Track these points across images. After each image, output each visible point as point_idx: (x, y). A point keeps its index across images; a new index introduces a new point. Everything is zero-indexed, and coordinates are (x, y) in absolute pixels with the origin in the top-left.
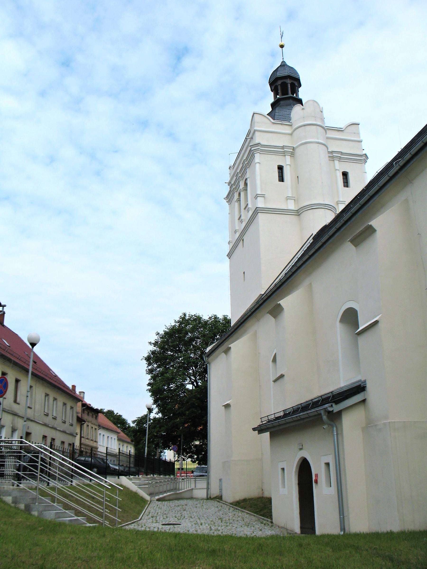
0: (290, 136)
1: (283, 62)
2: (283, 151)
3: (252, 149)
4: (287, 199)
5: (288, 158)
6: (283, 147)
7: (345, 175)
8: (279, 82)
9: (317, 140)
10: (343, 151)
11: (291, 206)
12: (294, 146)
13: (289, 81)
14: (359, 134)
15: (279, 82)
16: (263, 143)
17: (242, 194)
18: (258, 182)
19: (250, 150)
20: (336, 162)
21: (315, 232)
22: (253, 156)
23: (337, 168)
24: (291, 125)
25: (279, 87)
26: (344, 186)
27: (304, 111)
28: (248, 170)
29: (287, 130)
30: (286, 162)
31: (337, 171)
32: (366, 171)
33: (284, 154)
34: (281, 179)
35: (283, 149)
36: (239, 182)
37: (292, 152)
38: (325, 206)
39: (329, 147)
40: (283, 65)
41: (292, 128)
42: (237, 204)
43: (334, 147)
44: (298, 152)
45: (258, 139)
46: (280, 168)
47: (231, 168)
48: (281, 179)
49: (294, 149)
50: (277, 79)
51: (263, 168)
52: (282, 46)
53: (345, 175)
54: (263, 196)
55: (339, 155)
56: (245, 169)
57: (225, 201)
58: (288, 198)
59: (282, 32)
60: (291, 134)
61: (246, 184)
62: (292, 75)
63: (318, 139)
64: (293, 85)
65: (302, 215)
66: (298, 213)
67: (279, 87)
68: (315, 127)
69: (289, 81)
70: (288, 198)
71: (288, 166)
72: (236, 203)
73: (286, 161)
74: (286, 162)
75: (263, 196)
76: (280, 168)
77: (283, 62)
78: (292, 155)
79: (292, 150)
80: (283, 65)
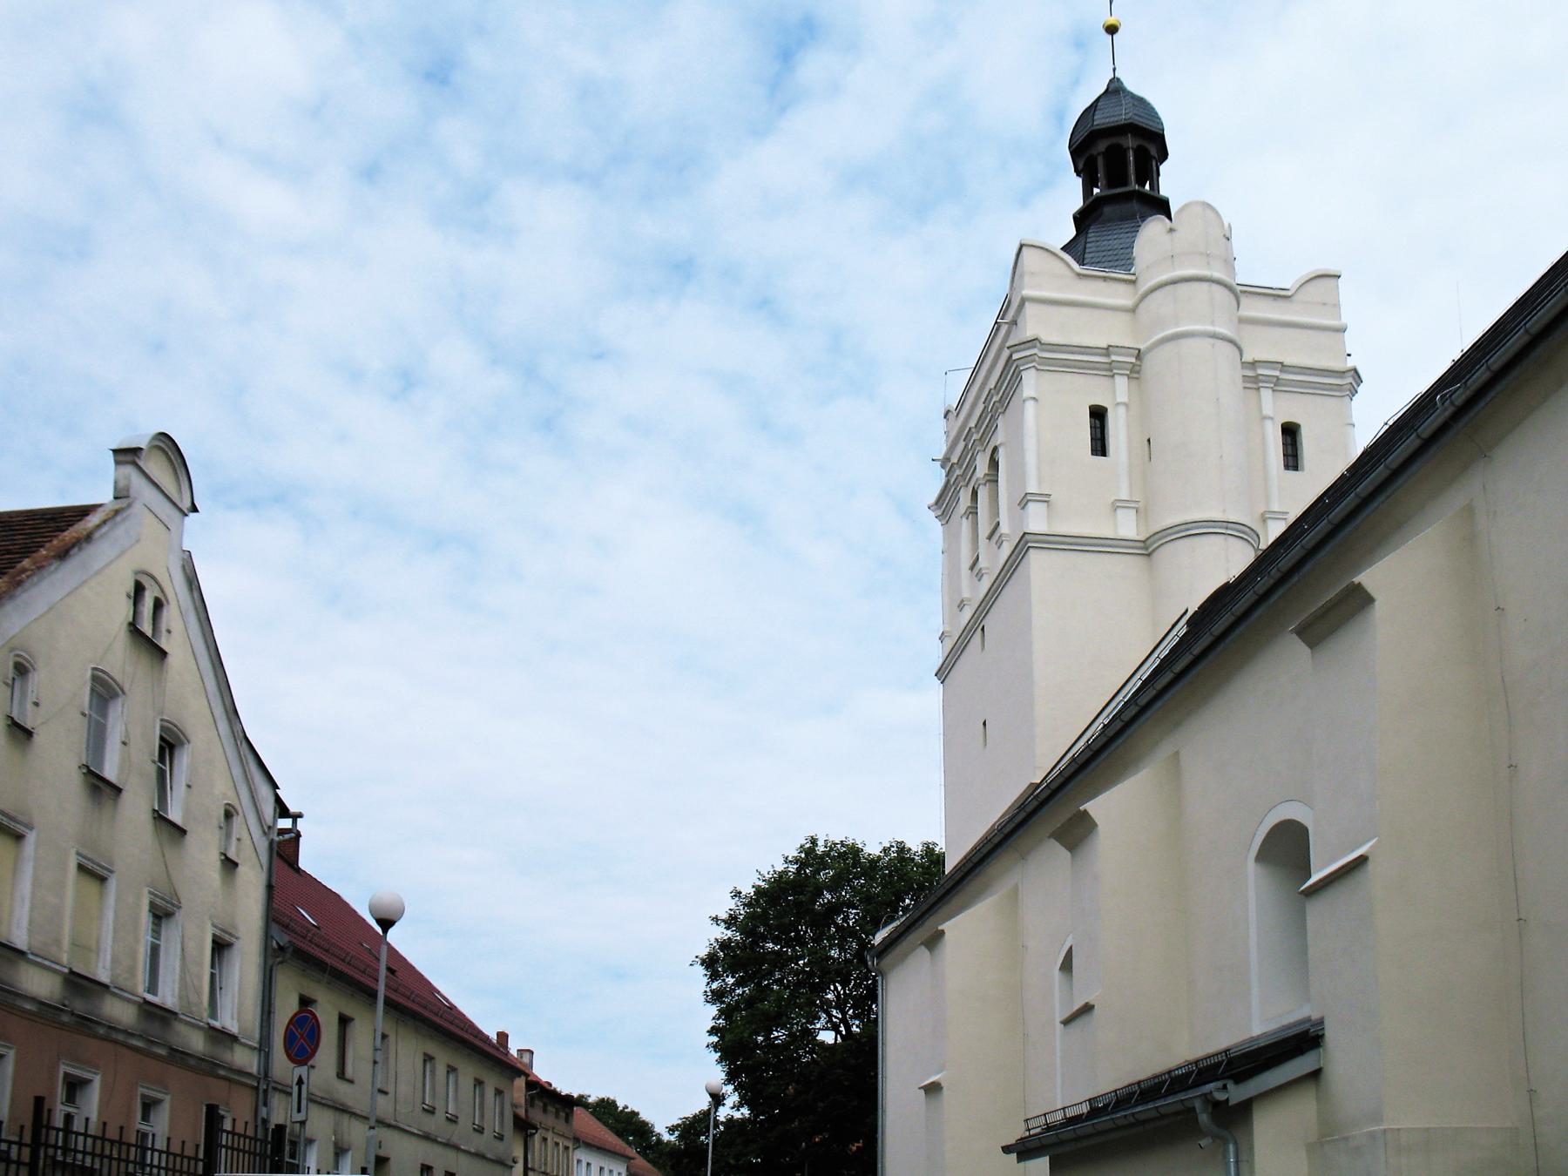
0: (1126, 317)
2: (1105, 362)
3: (1015, 356)
5: (1121, 383)
6: (1107, 351)
7: (1290, 432)
8: (1102, 146)
9: (1210, 328)
10: (1288, 361)
12: (1142, 347)
13: (1130, 142)
14: (1337, 306)
15: (1102, 146)
16: (1045, 338)
17: (983, 494)
20: (1266, 395)
21: (1193, 607)
22: (1016, 379)
23: (1267, 411)
24: (1134, 282)
25: (1100, 162)
29: (1120, 296)
30: (1116, 395)
31: (1268, 423)
32: (1354, 420)
33: (1110, 370)
34: (1100, 446)
35: (1108, 355)
36: (973, 458)
39: (1244, 347)
40: (1115, 89)
42: (966, 525)
43: (1260, 347)
44: (1151, 364)
45: (1035, 324)
46: (1098, 415)
48: (1100, 446)
51: (1047, 414)
52: (1112, 30)
53: (1290, 432)
54: (1044, 499)
55: (1277, 373)
57: (932, 514)
58: (1116, 506)
60: (1133, 310)
61: (994, 464)
63: (1212, 323)
65: (1165, 554)
66: (1147, 548)
67: (1100, 162)
68: (1205, 286)
69: (1130, 142)
70: (1116, 506)
71: (1122, 410)
74: (1116, 395)
75: (1044, 499)
76: (1098, 415)
78: (1135, 372)
80: (1115, 89)
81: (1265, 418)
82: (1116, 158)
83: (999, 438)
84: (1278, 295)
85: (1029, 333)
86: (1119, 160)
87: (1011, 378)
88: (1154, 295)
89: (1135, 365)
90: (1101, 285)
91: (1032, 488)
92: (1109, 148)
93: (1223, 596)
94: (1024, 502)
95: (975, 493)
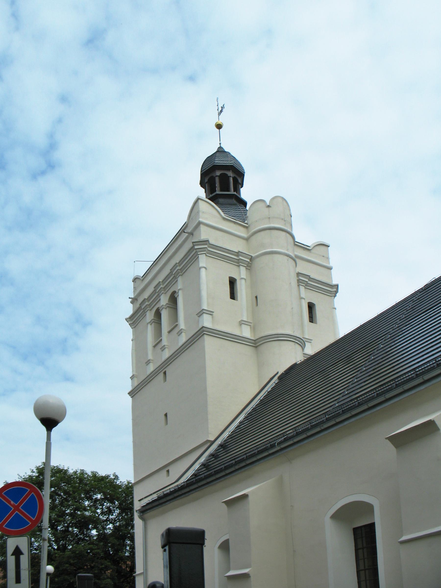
0: (244, 242)
1: (220, 148)
2: (236, 259)
3: (196, 247)
4: (241, 325)
5: (243, 270)
6: (238, 254)
7: (311, 307)
8: (218, 173)
9: (286, 252)
10: (312, 276)
11: (246, 332)
12: (253, 255)
13: (230, 174)
14: (328, 258)
15: (218, 173)
16: (212, 241)
17: (165, 314)
18: (204, 293)
19: (192, 249)
20: (302, 288)
21: (282, 370)
22: (195, 258)
23: (303, 295)
24: (247, 227)
25: (217, 180)
26: (310, 321)
27: (270, 208)
28: (180, 279)
29: (242, 232)
30: (241, 274)
31: (303, 300)
32: (336, 306)
33: (238, 263)
34: (233, 296)
35: (238, 256)
36: (159, 296)
37: (250, 263)
38: (296, 339)
39: (297, 265)
40: (221, 151)
41: (248, 232)
42: (150, 330)
43: (303, 268)
44: (258, 263)
45: (204, 234)
46: (232, 282)
47: (137, 280)
48: (233, 296)
49: (252, 259)
50: (215, 167)
51: (211, 276)
52: (219, 126)
53: (311, 307)
54: (210, 313)
55: (307, 280)
56: (175, 278)
57: (127, 324)
58: (241, 323)
59: (220, 105)
60: (247, 239)
61: (173, 299)
62: (235, 166)
63: (287, 250)
64: (235, 180)
65: (264, 348)
66: (256, 344)
67: (217, 180)
68: (284, 233)
69: (230, 174)
70: (241, 323)
71: (243, 281)
72: (149, 326)
73: (240, 273)
74: (241, 274)
75: (210, 313)
76: (232, 282)
77: (220, 148)
78: (249, 266)
79: (249, 260)
80: (221, 151)
81: (302, 298)
82: (224, 179)
83: (180, 284)
84: (305, 248)
85: (203, 237)
86: (222, 179)
87: (192, 257)
88: (262, 233)
89: (250, 263)
90: (232, 225)
91: (205, 307)
92: (221, 175)
93: (294, 367)
94: (201, 313)
95: (158, 314)
